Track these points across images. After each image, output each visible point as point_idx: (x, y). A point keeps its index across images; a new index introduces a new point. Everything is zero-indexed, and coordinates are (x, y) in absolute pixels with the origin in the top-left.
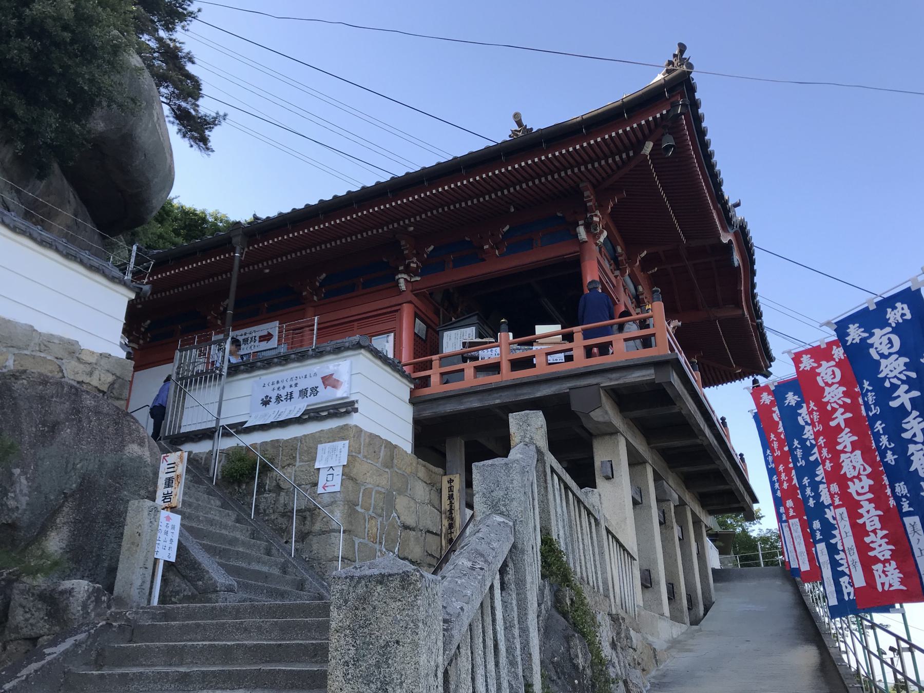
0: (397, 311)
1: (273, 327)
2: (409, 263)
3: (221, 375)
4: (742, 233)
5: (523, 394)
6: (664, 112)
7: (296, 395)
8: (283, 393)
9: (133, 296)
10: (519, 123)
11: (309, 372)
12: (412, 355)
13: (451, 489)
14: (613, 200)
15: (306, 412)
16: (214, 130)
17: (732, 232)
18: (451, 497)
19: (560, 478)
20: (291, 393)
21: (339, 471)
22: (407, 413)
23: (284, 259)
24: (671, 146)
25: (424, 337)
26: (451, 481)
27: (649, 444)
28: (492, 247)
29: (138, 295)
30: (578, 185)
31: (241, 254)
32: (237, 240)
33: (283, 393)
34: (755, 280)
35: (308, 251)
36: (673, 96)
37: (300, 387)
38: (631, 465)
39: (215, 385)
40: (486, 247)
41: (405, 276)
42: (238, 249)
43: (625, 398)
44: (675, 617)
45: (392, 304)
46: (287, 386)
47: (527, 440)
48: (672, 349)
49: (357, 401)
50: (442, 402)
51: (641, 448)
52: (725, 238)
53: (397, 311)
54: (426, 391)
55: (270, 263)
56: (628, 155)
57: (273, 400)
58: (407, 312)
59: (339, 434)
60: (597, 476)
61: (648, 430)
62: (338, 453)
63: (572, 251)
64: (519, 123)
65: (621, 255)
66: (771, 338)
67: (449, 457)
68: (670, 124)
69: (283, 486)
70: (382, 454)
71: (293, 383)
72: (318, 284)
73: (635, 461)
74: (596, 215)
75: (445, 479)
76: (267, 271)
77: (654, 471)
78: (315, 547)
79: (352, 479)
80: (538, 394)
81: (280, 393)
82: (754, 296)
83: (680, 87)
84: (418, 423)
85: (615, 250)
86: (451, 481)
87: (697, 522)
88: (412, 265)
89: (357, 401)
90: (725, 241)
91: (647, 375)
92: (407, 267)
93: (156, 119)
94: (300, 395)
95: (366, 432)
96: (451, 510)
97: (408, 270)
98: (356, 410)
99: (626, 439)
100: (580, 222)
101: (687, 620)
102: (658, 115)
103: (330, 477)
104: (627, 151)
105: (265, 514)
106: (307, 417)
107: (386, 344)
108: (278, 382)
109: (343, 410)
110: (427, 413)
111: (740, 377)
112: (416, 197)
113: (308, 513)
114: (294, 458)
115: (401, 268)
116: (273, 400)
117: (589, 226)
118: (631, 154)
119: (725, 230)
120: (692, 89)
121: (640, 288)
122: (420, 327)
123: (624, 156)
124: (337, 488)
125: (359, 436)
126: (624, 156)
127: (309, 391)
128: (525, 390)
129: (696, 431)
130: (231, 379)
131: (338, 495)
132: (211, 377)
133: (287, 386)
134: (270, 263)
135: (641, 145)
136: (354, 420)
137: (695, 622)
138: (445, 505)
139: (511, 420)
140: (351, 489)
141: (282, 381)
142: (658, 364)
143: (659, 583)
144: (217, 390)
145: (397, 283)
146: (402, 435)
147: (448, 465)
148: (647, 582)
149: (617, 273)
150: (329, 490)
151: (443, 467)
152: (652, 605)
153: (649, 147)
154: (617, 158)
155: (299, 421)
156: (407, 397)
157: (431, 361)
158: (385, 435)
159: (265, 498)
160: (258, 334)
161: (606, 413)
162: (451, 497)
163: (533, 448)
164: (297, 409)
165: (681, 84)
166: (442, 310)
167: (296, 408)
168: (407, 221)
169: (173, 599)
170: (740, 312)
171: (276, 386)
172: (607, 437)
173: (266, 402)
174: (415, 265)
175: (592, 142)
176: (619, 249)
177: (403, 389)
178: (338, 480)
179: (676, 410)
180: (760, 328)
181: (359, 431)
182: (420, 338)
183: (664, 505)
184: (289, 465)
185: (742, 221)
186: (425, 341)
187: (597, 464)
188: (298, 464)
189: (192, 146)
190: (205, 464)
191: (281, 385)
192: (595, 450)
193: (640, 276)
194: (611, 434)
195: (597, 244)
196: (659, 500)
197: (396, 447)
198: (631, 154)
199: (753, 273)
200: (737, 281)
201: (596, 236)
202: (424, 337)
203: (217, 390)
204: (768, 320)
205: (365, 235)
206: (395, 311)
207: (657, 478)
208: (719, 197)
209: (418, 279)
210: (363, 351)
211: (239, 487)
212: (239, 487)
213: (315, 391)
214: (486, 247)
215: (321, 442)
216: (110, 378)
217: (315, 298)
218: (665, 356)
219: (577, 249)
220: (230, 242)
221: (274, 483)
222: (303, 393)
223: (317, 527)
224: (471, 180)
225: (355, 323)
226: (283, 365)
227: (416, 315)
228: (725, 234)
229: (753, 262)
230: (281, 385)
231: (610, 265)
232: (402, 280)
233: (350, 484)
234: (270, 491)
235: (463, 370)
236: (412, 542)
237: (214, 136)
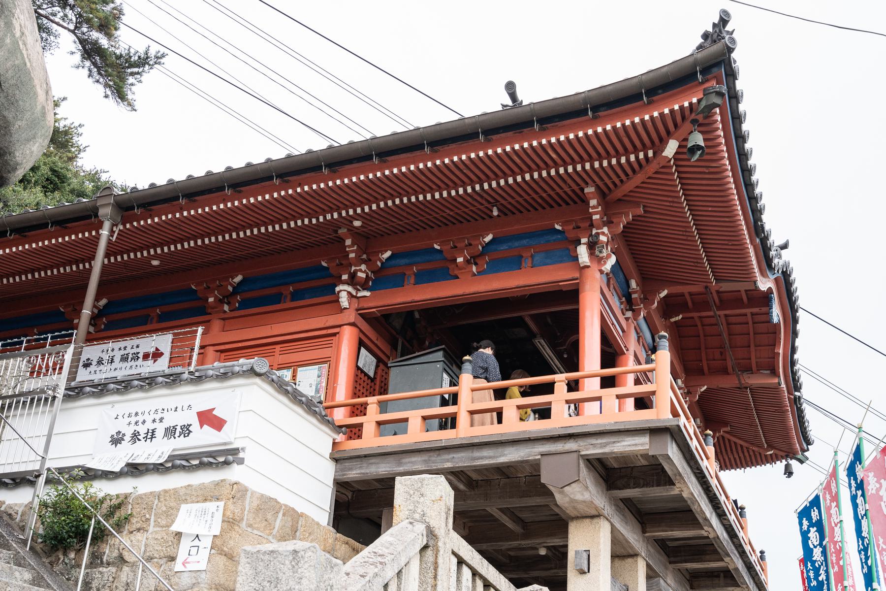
0: (334, 335)
1: (164, 342)
2: (356, 272)
3: (54, 398)
4: (785, 281)
5: (482, 458)
6: (695, 100)
7: (160, 433)
8: (142, 430)
10: (513, 96)
11: (182, 404)
12: (351, 393)
14: (627, 215)
15: (171, 458)
16: (145, 77)
17: (772, 277)
19: (475, 573)
20: (153, 431)
21: (207, 542)
22: (327, 472)
23: (179, 247)
24: (699, 147)
25: (372, 374)
27: (644, 532)
30: (582, 190)
31: (112, 232)
32: (105, 212)
33: (142, 430)
34: (797, 344)
35: (213, 239)
36: (707, 81)
37: (167, 423)
38: (615, 556)
39: (43, 412)
41: (350, 289)
42: (107, 225)
43: (611, 474)
45: (327, 325)
46: (149, 419)
47: (417, 516)
48: (675, 414)
49: (243, 449)
50: (373, 460)
51: (632, 537)
52: (765, 284)
53: (334, 335)
54: (355, 445)
55: (159, 251)
56: (646, 155)
57: (127, 438)
58: (347, 339)
59: (207, 495)
60: (569, 568)
61: (643, 516)
62: (209, 518)
63: (570, 277)
64: (513, 96)
65: (635, 292)
66: (809, 413)
68: (699, 118)
69: (127, 558)
70: (278, 523)
71: (157, 417)
72: (230, 288)
73: (621, 554)
74: (603, 233)
76: (155, 263)
77: (648, 565)
79: (222, 553)
80: (502, 460)
81: (137, 428)
82: (793, 363)
83: (712, 66)
84: (341, 485)
85: (628, 286)
88: (360, 274)
89: (243, 449)
91: (640, 444)
92: (353, 276)
93: (18, 34)
94: (165, 435)
95: (253, 493)
97: (353, 280)
98: (241, 462)
99: (612, 525)
103: (194, 550)
104: (645, 149)
106: (170, 465)
107: (309, 380)
108: (137, 414)
109: (221, 459)
110: (355, 473)
111: (772, 460)
112: (362, 177)
114: (148, 520)
116: (127, 438)
120: (732, 75)
122: (367, 361)
124: (203, 566)
125: (243, 496)
127: (179, 429)
128: (486, 452)
129: (701, 521)
130: (70, 405)
131: (203, 575)
132: (39, 400)
133: (149, 419)
134: (159, 251)
135: (663, 142)
136: (234, 473)
140: (221, 566)
141: (143, 413)
142: (655, 432)
144: (46, 419)
149: (629, 314)
150: (190, 567)
153: (671, 148)
154: (632, 158)
155: (159, 469)
156: (328, 449)
157: (366, 404)
158: (285, 499)
159: (101, 573)
160: (141, 351)
161: (580, 492)
163: (421, 528)
164: (159, 453)
165: (717, 64)
166: (398, 337)
167: (156, 451)
168: (351, 212)
170: (776, 381)
171: (133, 419)
173: (116, 440)
174: (363, 275)
176: (633, 284)
177: (322, 439)
178: (204, 554)
179: (675, 491)
180: (797, 402)
182: (366, 374)
184: (139, 530)
185: (787, 265)
186: (373, 380)
187: (571, 555)
189: (106, 96)
190: (22, 521)
191: (140, 418)
192: (570, 536)
193: (658, 321)
194: (592, 517)
195: (601, 272)
197: (301, 515)
198: (650, 153)
199: (795, 334)
200: (774, 344)
201: (600, 260)
202: (372, 374)
203: (46, 419)
204: (809, 391)
205: (292, 224)
206: (331, 335)
207: (651, 575)
208: (758, 230)
210: (257, 380)
211: (65, 554)
212: (65, 554)
213: (186, 430)
214: (460, 260)
215: (185, 501)
217: (226, 308)
218: (664, 421)
219: (577, 275)
220: (96, 216)
221: (115, 554)
222: (170, 432)
224: (438, 162)
225: (278, 347)
226: (147, 391)
227: (361, 344)
228: (764, 280)
229: (795, 321)
230: (140, 418)
231: (621, 303)
232: (344, 292)
233: (221, 560)
234: (108, 564)
235: (406, 420)
237: (144, 87)
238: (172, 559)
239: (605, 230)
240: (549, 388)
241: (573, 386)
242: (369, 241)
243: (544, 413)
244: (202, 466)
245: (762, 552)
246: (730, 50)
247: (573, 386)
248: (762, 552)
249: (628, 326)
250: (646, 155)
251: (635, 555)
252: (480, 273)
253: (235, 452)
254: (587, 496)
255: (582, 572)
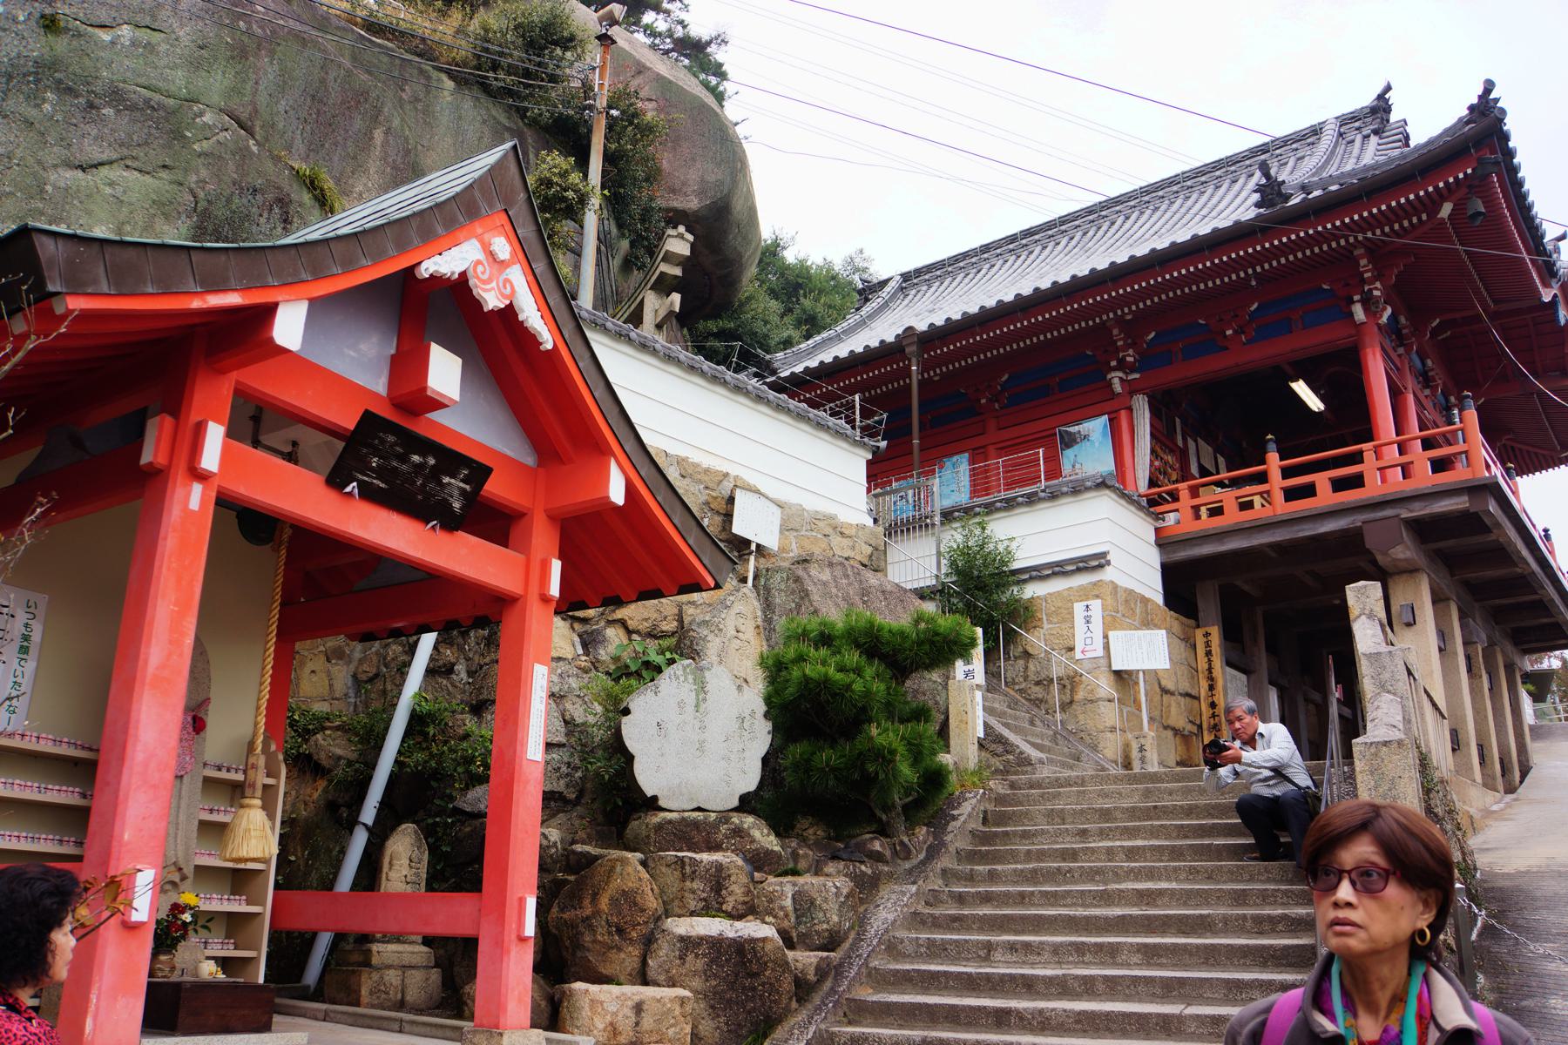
6: (1469, 171)
9: (870, 457)
13: (1208, 644)
18: (1209, 653)
22: (1154, 558)
26: (1207, 635)
27: (1452, 575)
28: (1235, 332)
29: (874, 453)
40: (1229, 332)
41: (1120, 374)
44: (1489, 784)
56: (1420, 219)
59: (1085, 594)
67: (1201, 605)
68: (1477, 185)
73: (1438, 600)
75: (1199, 633)
78: (1081, 717)
86: (1207, 635)
87: (1510, 668)
90: (1547, 299)
96: (1210, 670)
98: (1108, 563)
100: (1356, 298)
101: (1501, 788)
102: (1461, 176)
105: (1014, 683)
113: (1070, 682)
115: (1113, 363)
117: (1367, 302)
118: (1424, 217)
119: (1546, 285)
121: (1429, 363)
123: (1415, 220)
126: (1415, 220)
135: (1439, 207)
136: (1108, 574)
137: (1510, 789)
138: (1202, 664)
139: (1348, 592)
143: (1468, 744)
145: (1110, 384)
146: (1152, 587)
147: (1201, 615)
148: (1457, 744)
149: (1401, 350)
150: (1089, 655)
151: (1197, 619)
152: (1463, 769)
153: (1446, 210)
162: (1209, 653)
169: (335, 853)
172: (1405, 576)
175: (1375, 211)
179: (1493, 537)
181: (1115, 587)
183: (1471, 649)
188: (1046, 626)
196: (1466, 644)
198: (1424, 217)
209: (1137, 376)
216: (869, 550)
223: (1080, 695)
232: (1116, 378)
236: (1174, 710)
238: (1071, 649)
239: (1378, 285)
240: (1357, 458)
241: (1377, 452)
242: (1133, 329)
243: (1357, 481)
244: (1079, 570)
245: (1546, 531)
246: (1501, 121)
247: (1377, 452)
248: (1546, 531)
249: (1402, 362)
250: (1420, 219)
251: (1448, 599)
252: (1250, 341)
253: (1103, 555)
254: (1408, 554)
255: (1409, 625)
